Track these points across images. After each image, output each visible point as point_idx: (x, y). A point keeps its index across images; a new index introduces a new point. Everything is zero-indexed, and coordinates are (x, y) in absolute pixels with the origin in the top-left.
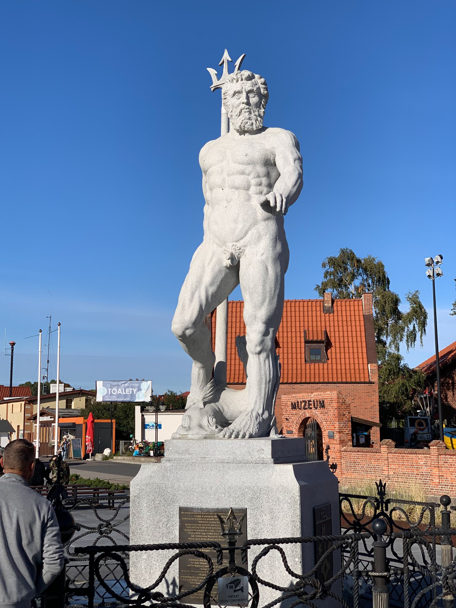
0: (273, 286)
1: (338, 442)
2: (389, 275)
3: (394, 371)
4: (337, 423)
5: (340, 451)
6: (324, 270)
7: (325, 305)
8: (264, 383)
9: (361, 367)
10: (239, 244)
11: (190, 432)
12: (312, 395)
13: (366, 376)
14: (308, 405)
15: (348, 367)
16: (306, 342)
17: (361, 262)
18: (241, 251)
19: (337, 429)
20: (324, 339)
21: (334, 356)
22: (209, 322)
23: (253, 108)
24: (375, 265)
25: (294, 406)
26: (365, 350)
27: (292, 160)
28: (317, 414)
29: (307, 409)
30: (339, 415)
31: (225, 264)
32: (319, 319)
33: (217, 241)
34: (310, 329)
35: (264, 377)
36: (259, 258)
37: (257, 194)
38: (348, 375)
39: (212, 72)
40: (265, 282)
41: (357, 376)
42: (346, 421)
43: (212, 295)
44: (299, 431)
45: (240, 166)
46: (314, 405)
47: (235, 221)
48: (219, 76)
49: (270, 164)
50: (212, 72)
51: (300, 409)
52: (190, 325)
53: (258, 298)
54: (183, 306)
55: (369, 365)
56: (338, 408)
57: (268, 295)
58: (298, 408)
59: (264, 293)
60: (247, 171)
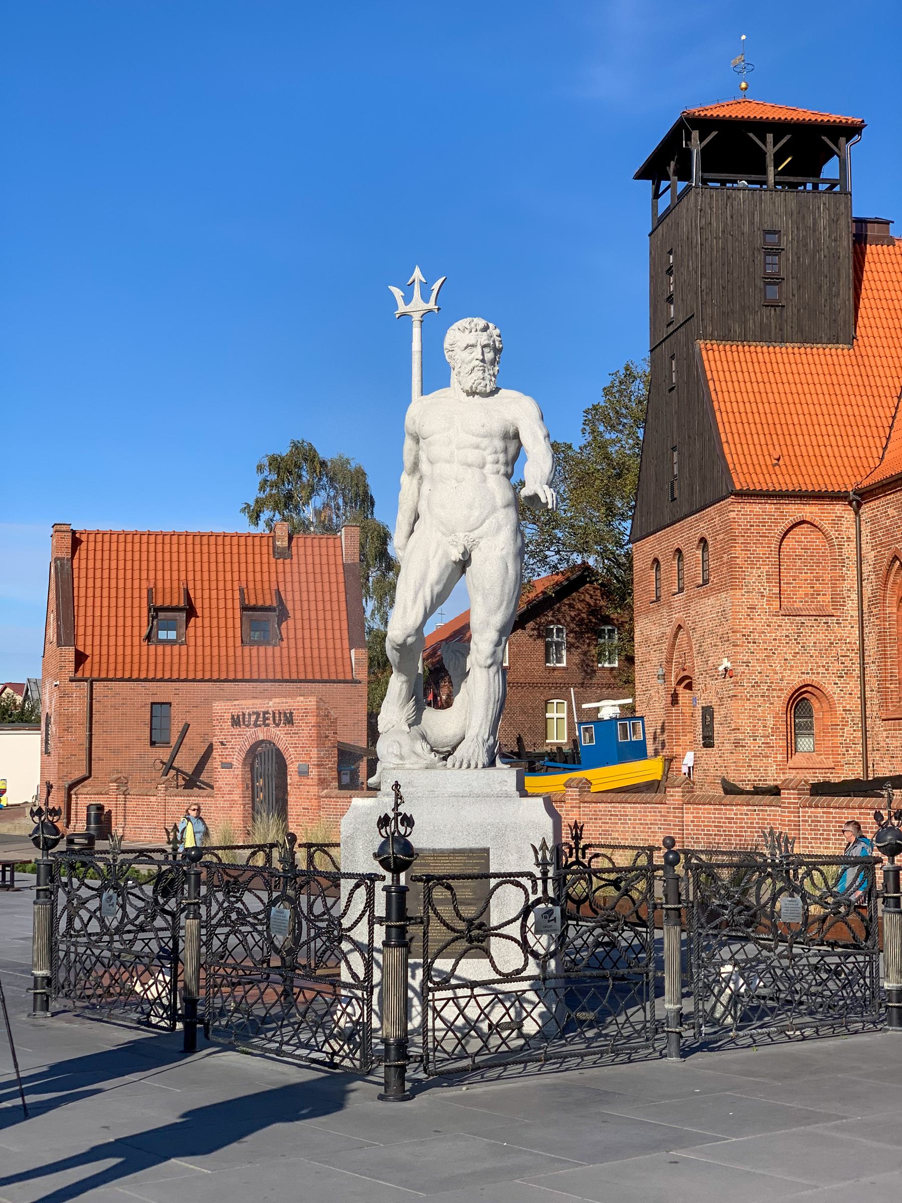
0: (512, 587)
1: (316, 781)
2: (373, 491)
3: (378, 660)
4: (314, 753)
5: (319, 796)
6: (260, 478)
7: (277, 543)
8: (492, 703)
9: (339, 655)
10: (473, 535)
11: (407, 762)
12: (271, 703)
13: (348, 669)
14: (262, 719)
15: (316, 654)
16: (244, 608)
17: (327, 466)
18: (475, 543)
19: (314, 760)
20: (275, 605)
21: (292, 635)
22: (67, 567)
23: (487, 366)
24: (350, 471)
25: (236, 722)
26: (345, 625)
27: (541, 437)
28: (280, 736)
29: (260, 726)
30: (319, 736)
31: (453, 559)
32: (265, 568)
33: (442, 528)
34: (251, 585)
35: (492, 695)
36: (498, 553)
37: (493, 473)
38: (317, 668)
39: (397, 293)
40: (504, 582)
41: (332, 669)
42: (329, 747)
43: (437, 596)
44: (244, 764)
45: (475, 438)
46: (274, 720)
47: (470, 507)
48: (408, 300)
49: (513, 437)
50: (397, 293)
51: (248, 726)
52: (413, 632)
53: (493, 601)
54: (405, 608)
55: (353, 651)
56: (318, 726)
57: (506, 598)
58: (244, 724)
59: (502, 595)
60: (483, 446)
